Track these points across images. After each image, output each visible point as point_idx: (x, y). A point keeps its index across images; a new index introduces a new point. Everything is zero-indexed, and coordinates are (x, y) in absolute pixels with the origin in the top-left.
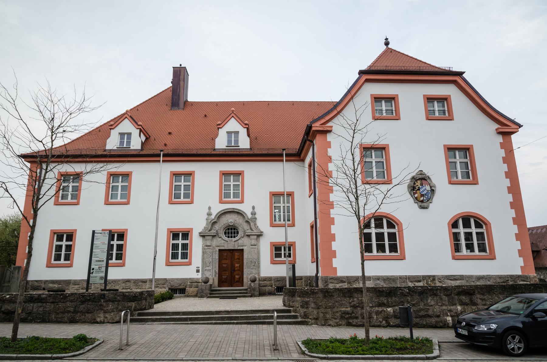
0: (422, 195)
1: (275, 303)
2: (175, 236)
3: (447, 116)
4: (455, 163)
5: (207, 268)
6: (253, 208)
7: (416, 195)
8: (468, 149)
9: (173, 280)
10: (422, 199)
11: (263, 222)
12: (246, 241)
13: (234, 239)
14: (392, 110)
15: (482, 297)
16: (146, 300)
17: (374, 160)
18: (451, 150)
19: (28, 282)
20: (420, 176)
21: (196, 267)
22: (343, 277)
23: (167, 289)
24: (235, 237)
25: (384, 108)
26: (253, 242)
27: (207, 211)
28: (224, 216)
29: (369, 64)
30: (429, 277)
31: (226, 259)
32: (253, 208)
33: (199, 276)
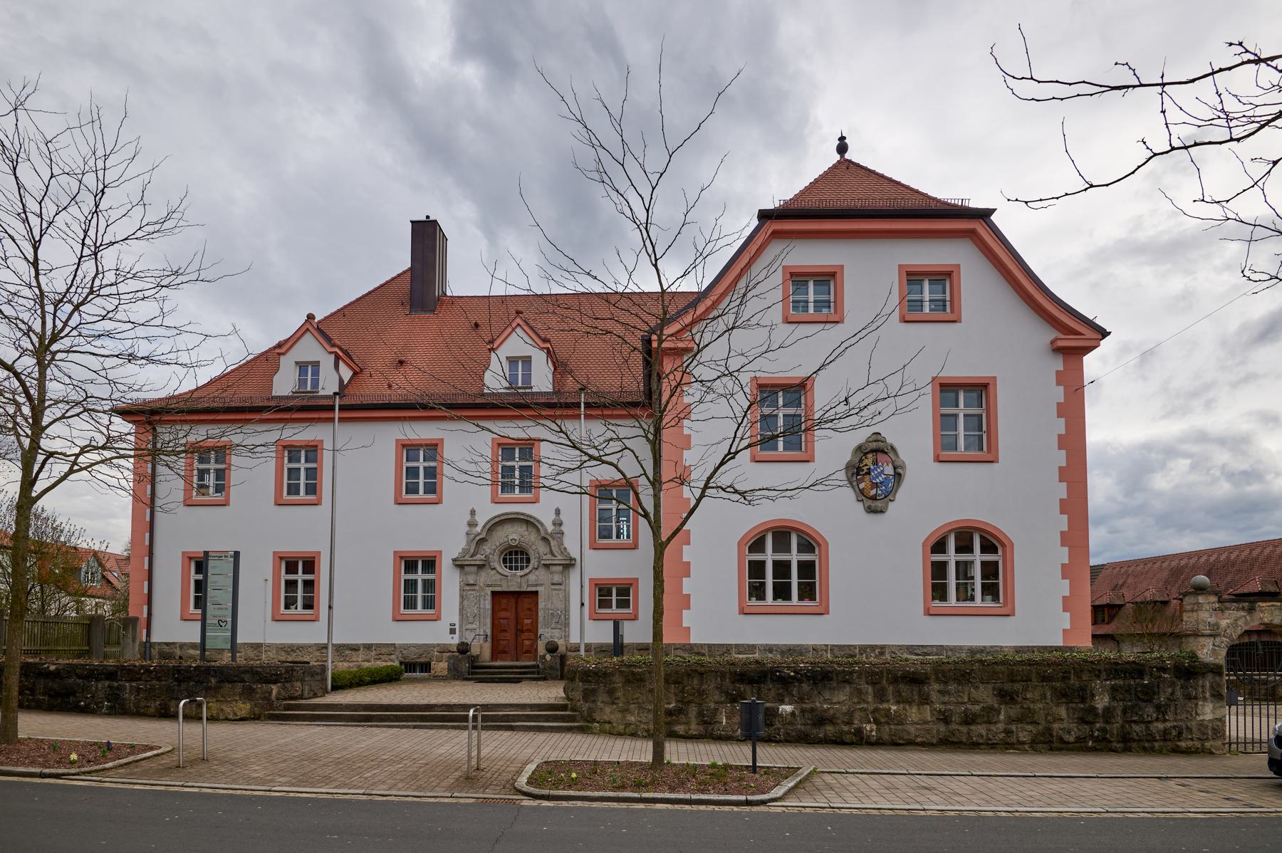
0: (876, 486)
1: (552, 693)
2: (410, 565)
3: (946, 311)
4: (956, 416)
5: (470, 626)
6: (558, 512)
7: (862, 486)
8: (986, 386)
9: (407, 647)
10: (873, 492)
11: (574, 540)
12: (542, 575)
13: (520, 573)
14: (944, 301)
15: (942, 687)
16: (302, 681)
17: (961, 410)
18: (947, 389)
19: (152, 645)
20: (874, 445)
21: (451, 621)
22: (702, 646)
23: (397, 664)
24: (522, 568)
25: (927, 296)
26: (557, 578)
27: (468, 518)
28: (499, 528)
29: (789, 196)
30: (873, 647)
31: (506, 610)
32: (558, 512)
33: (455, 640)
